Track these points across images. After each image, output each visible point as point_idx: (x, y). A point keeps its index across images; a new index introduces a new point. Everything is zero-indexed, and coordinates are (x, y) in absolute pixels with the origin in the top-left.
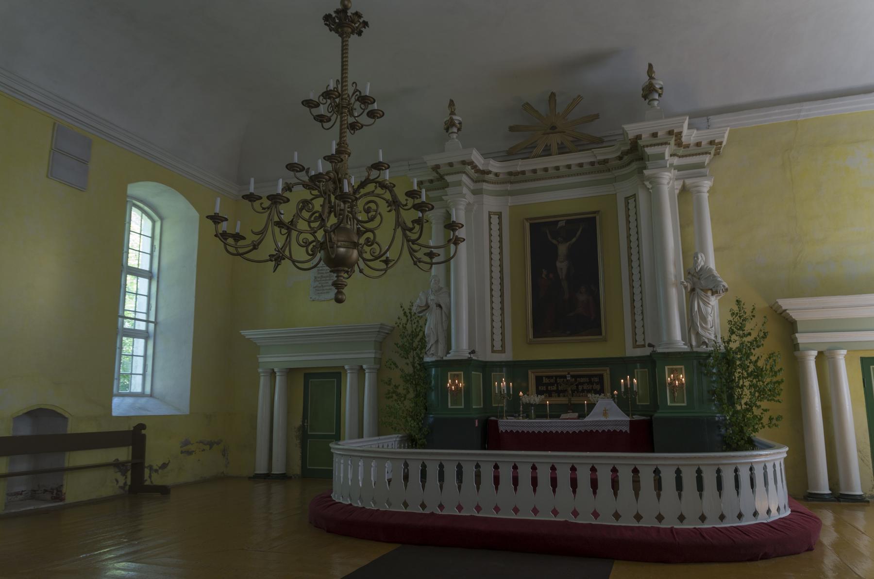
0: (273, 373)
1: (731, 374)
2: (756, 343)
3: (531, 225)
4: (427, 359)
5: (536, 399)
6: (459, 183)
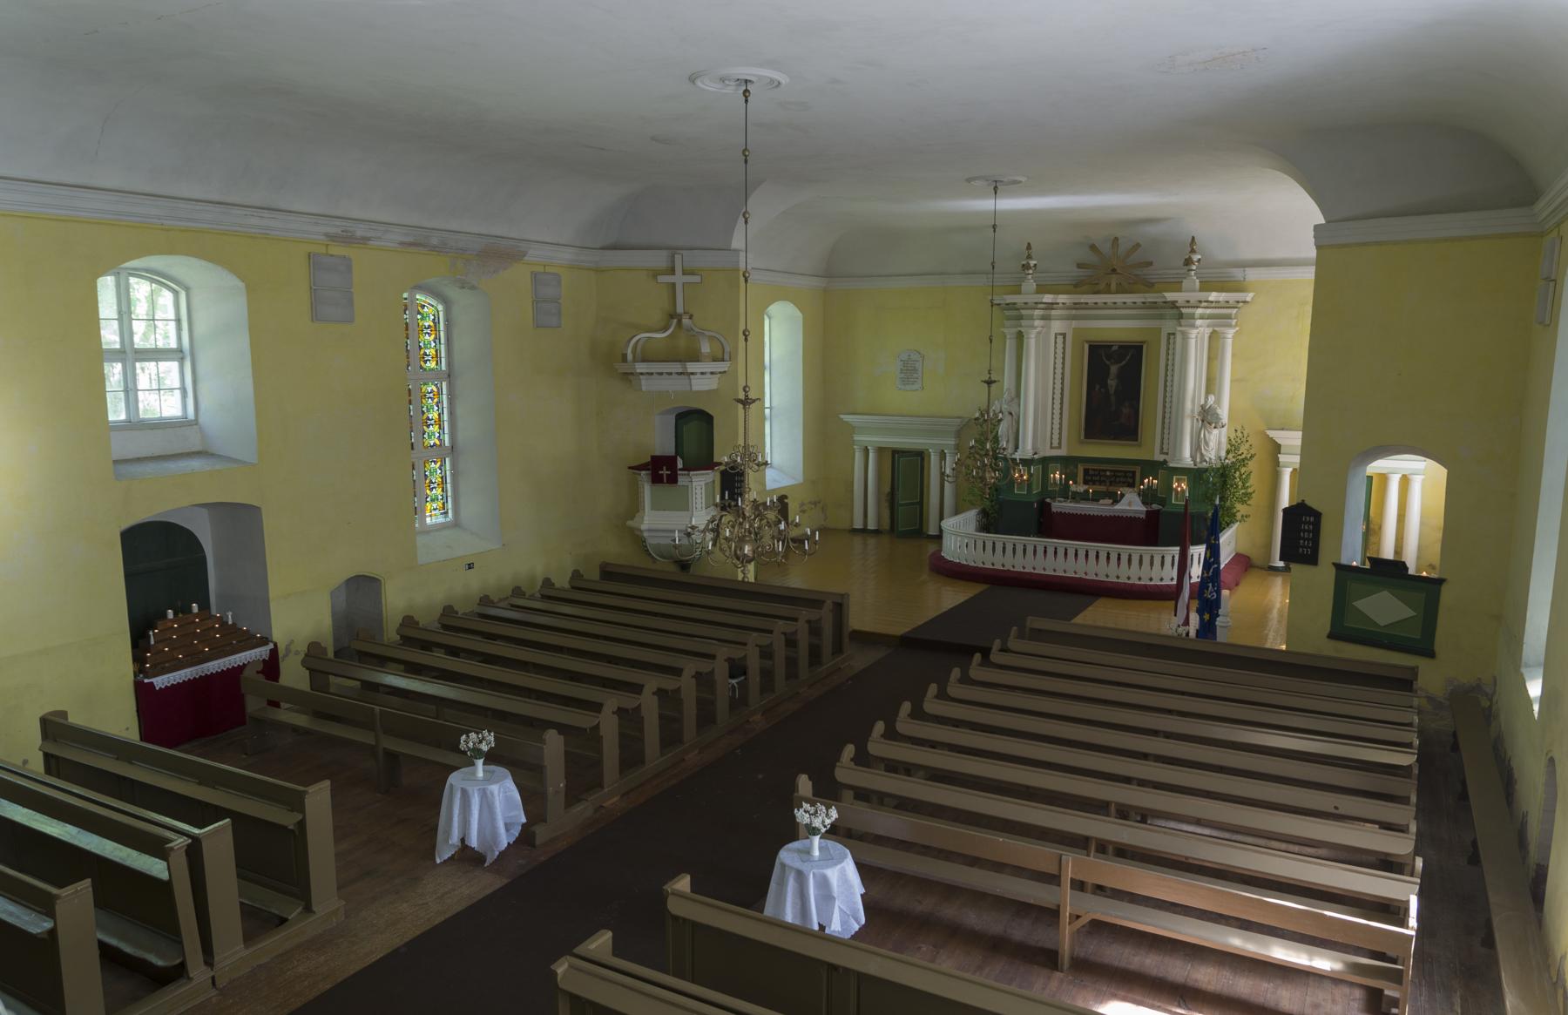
0: (866, 450)
5: (1081, 488)
6: (1031, 318)
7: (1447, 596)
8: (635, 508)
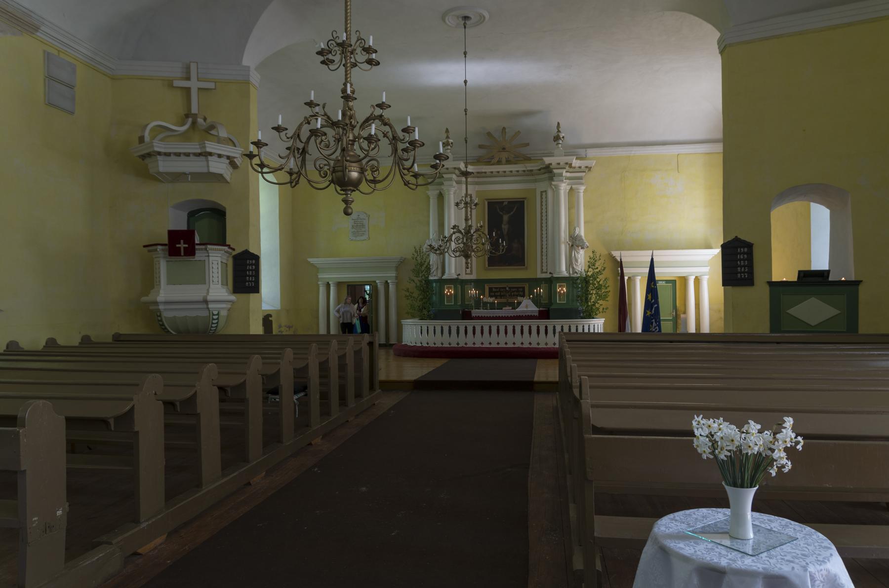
0: (328, 285)
1: (587, 287)
2: (600, 273)
3: (489, 203)
4: (431, 278)
5: (491, 300)
6: (450, 179)
7: (863, 293)
8: (150, 282)
